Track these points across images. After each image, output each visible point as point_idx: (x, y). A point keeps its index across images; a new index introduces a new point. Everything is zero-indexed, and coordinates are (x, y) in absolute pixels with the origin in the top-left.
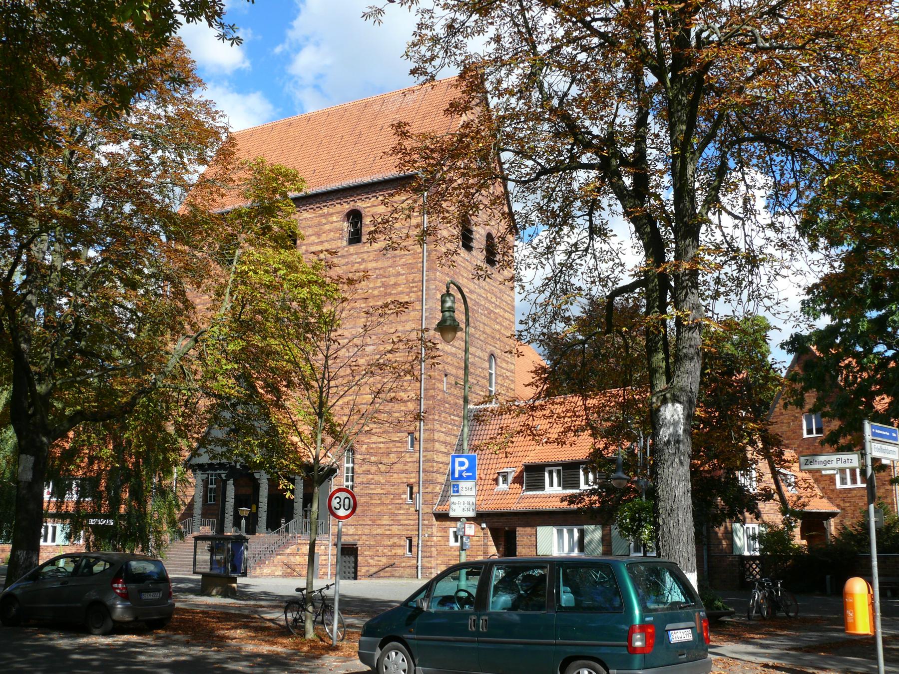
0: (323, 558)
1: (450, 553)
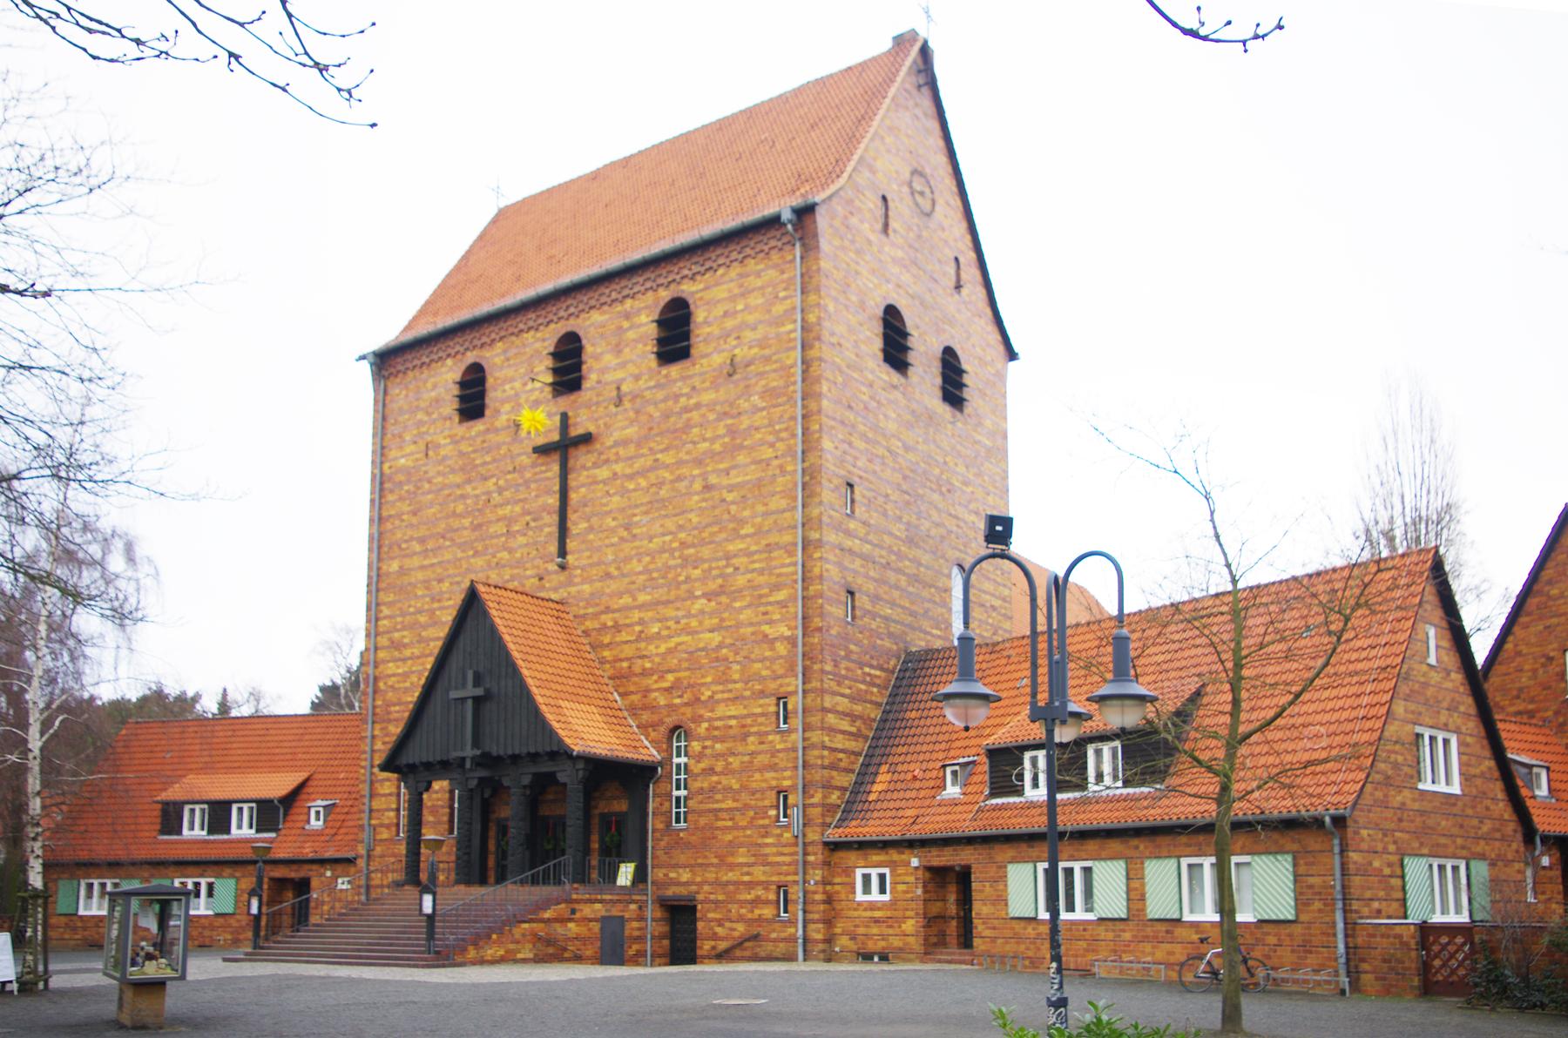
0: (635, 924)
1: (856, 914)
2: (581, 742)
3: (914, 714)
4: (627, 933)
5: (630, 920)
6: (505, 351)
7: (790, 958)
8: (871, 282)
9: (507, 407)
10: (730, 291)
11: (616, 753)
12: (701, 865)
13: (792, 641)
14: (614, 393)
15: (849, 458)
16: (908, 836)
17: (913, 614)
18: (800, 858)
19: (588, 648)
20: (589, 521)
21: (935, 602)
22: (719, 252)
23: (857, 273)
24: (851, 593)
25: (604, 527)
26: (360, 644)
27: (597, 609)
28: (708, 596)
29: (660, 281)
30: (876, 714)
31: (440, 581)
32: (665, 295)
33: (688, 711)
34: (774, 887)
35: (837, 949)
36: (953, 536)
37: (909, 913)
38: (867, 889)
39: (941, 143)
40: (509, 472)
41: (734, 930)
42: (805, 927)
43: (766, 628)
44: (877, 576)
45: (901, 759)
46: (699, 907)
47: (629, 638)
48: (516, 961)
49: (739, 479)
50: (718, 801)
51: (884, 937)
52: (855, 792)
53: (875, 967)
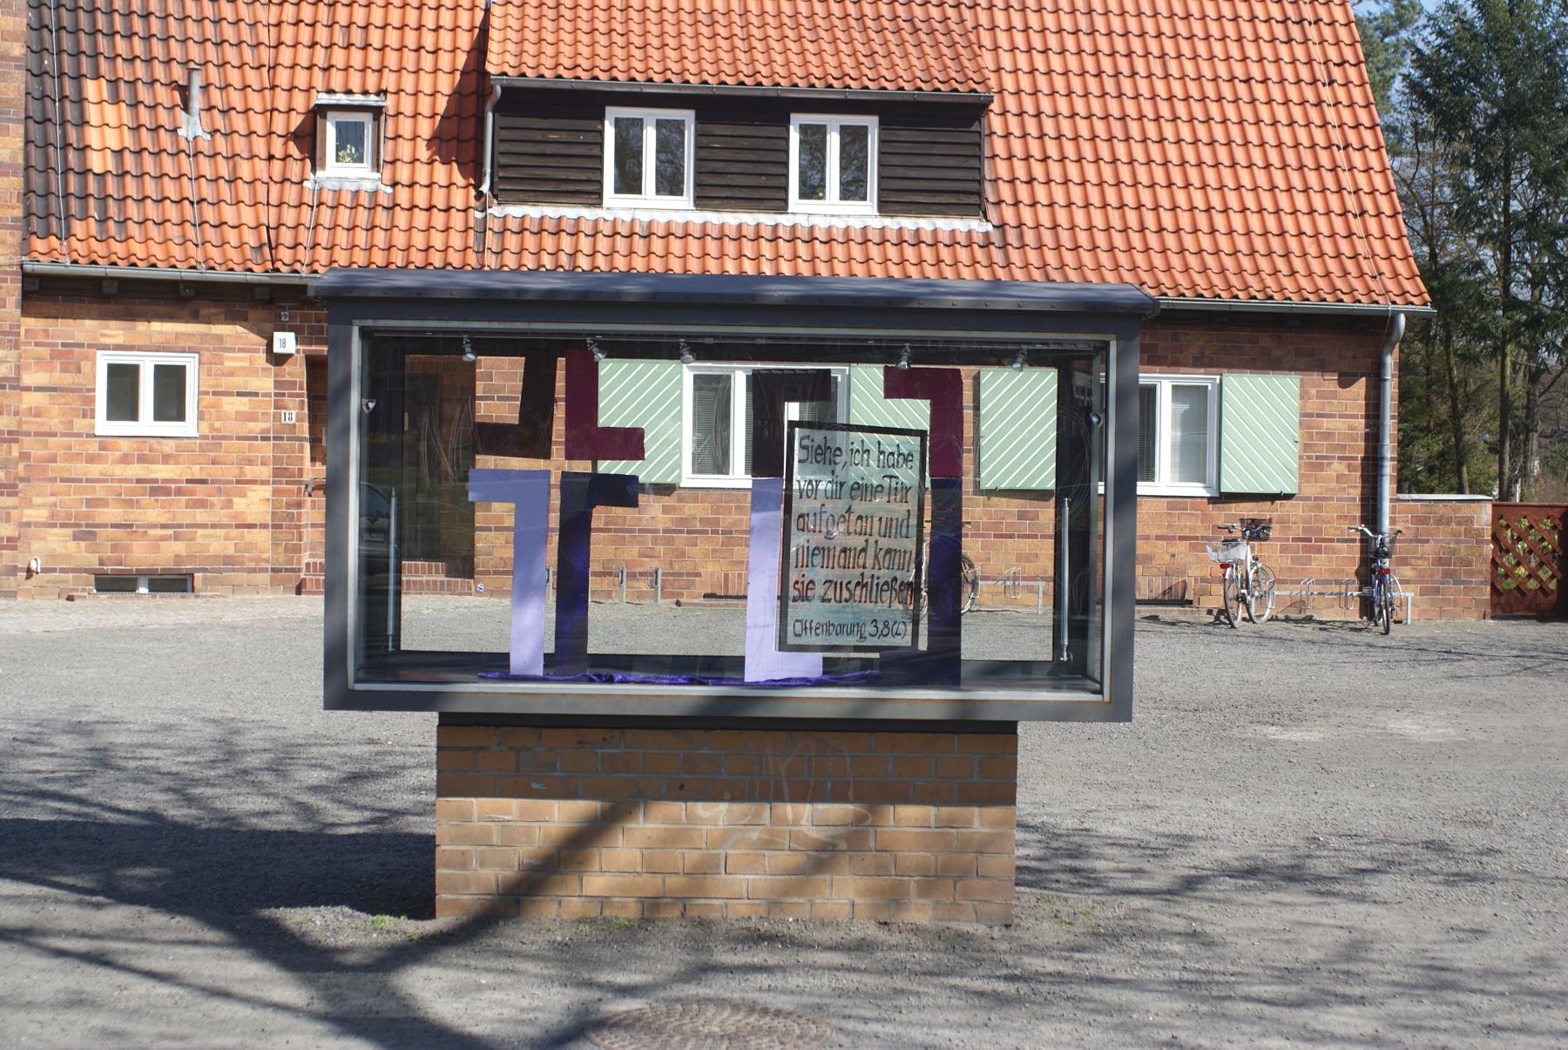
51: (177, 530)
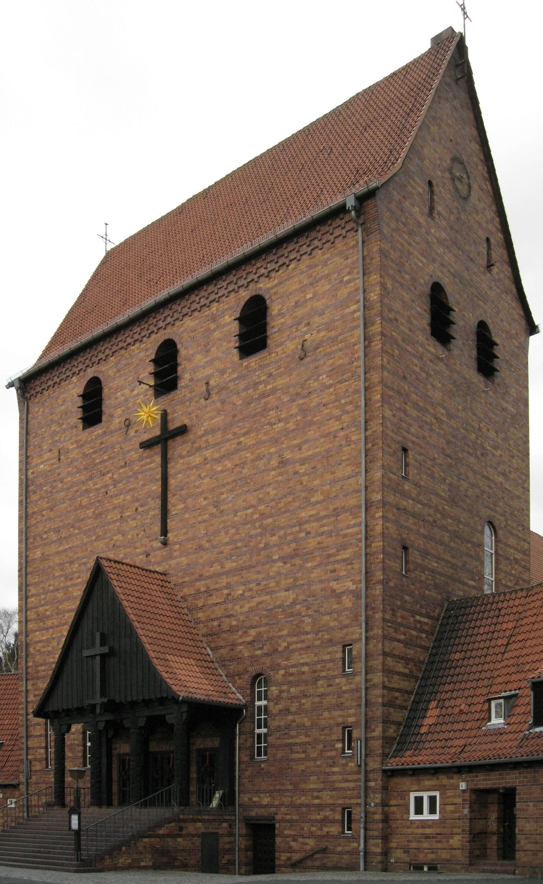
0: (227, 839)
1: (409, 831)
2: (184, 689)
3: (458, 656)
4: (220, 846)
5: (223, 835)
6: (116, 364)
7: (352, 867)
8: (421, 262)
9: (119, 411)
10: (300, 282)
11: (212, 698)
12: (279, 791)
13: (356, 594)
14: (204, 388)
15: (404, 425)
16: (458, 763)
17: (454, 567)
18: (362, 784)
19: (185, 611)
20: (185, 502)
21: (471, 556)
22: (291, 247)
23: (410, 253)
24: (405, 548)
25: (198, 506)
26: (15, 627)
27: (193, 577)
28: (284, 560)
29: (240, 283)
30: (424, 657)
31: (71, 563)
32: (245, 295)
33: (268, 661)
34: (340, 809)
35: (392, 860)
36: (485, 496)
37: (455, 830)
38: (419, 810)
39: (475, 132)
40: (122, 467)
41: (307, 844)
42: (365, 842)
43: (334, 585)
44: (426, 533)
45: (448, 695)
46: (277, 825)
47: (218, 601)
48: (140, 868)
49: (310, 453)
50: (292, 737)
51: (433, 851)
52: (408, 726)
53: (424, 877)
